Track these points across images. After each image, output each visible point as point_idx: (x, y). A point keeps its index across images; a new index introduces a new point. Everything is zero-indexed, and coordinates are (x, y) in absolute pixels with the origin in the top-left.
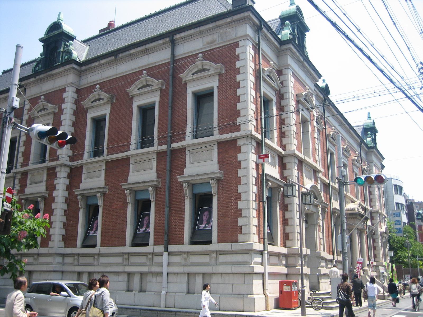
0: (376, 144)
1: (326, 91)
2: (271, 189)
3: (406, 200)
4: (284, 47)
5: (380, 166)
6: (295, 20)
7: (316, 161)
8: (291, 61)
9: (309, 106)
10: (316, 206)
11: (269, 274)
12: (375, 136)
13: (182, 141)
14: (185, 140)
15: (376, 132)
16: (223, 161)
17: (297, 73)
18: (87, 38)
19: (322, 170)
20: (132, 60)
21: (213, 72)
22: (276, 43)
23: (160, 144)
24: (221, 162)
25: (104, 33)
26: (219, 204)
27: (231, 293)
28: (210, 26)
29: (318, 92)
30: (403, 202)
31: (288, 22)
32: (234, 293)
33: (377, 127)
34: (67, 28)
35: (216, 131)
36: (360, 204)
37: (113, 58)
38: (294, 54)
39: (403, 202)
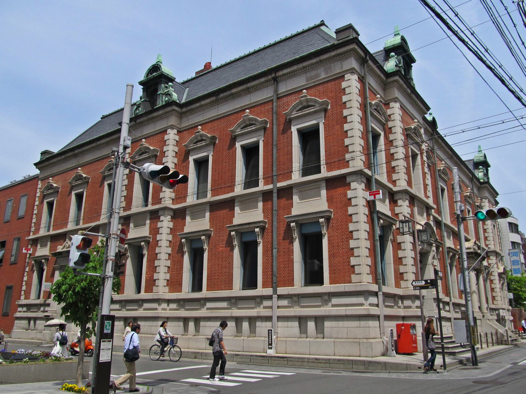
0: (488, 178)
1: (433, 124)
2: (383, 228)
3: (522, 239)
4: (391, 79)
5: (494, 203)
6: (401, 50)
7: (428, 197)
8: (397, 94)
9: (418, 140)
10: (431, 245)
11: (278, 317)
12: (487, 171)
13: (288, 179)
14: (291, 179)
15: (488, 166)
16: (332, 199)
17: (404, 106)
18: (185, 80)
19: (435, 207)
20: (250, 93)
21: (318, 108)
22: (382, 76)
23: (266, 184)
24: (330, 200)
25: (200, 75)
26: (329, 244)
27: (346, 337)
28: (314, 61)
29: (426, 125)
30: (519, 241)
31: (393, 54)
32: (349, 337)
33: (489, 160)
34: (166, 69)
35: (323, 168)
36: (475, 243)
37: (213, 98)
38: (401, 86)
39: (519, 241)
